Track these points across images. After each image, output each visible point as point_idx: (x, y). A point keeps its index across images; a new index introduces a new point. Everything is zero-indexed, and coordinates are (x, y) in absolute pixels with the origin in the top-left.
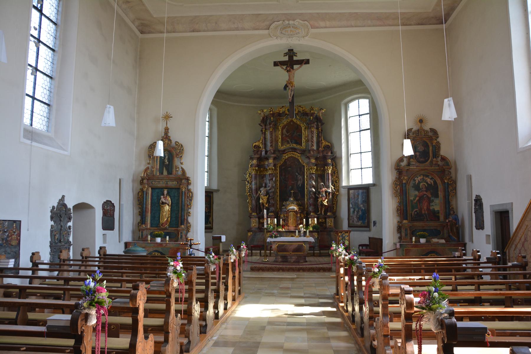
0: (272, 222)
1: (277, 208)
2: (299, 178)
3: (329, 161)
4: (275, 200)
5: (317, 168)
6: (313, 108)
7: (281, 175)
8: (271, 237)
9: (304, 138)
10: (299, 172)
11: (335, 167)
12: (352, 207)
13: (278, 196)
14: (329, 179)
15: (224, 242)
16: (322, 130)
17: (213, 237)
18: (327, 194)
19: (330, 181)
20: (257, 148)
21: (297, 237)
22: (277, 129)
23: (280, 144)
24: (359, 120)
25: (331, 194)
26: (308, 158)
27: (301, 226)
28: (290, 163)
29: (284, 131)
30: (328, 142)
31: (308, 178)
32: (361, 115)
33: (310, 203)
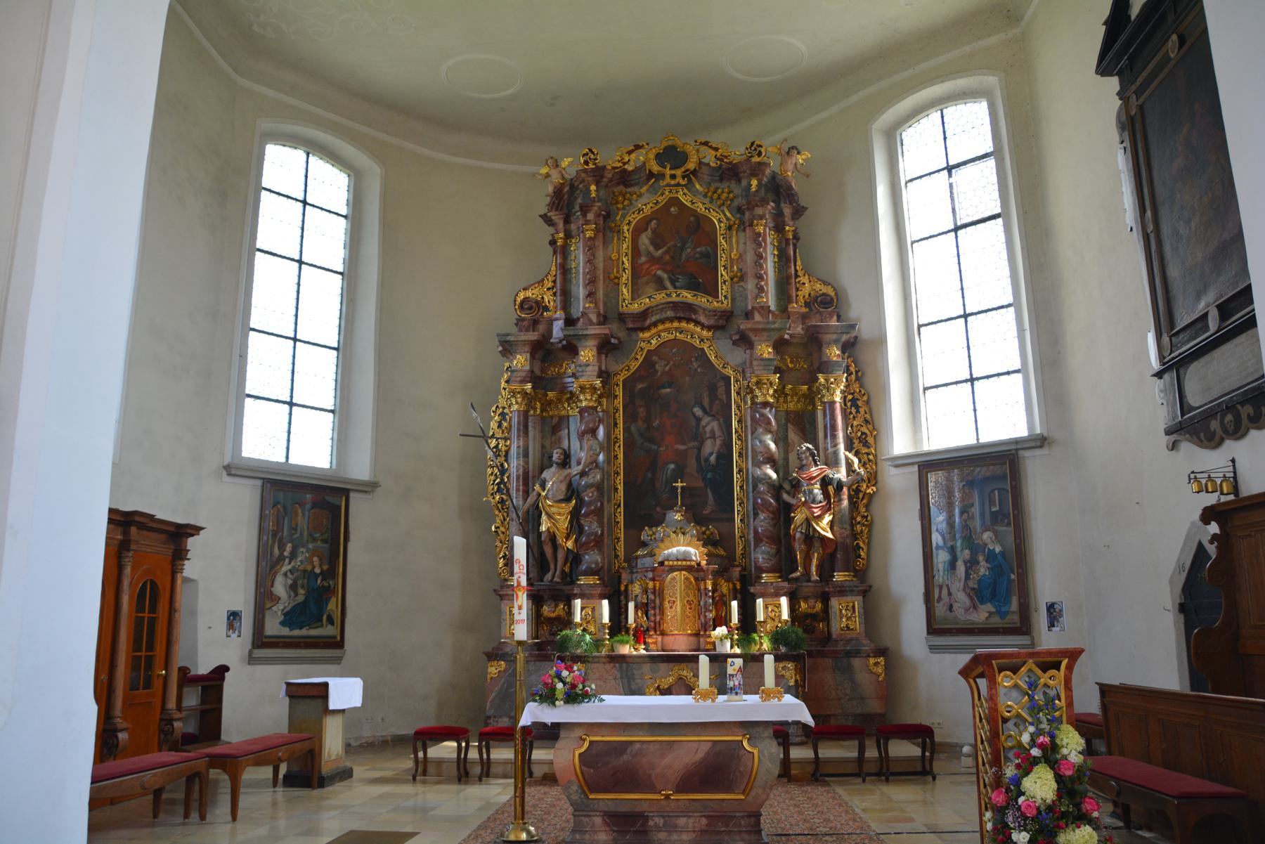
0: (593, 617)
1: (616, 556)
2: (708, 429)
3: (834, 353)
4: (606, 520)
5: (784, 388)
6: (760, 146)
7: (630, 416)
8: (548, 697)
9: (725, 268)
10: (706, 402)
11: (857, 379)
12: (941, 543)
13: (619, 506)
14: (834, 427)
15: (355, 709)
16: (796, 237)
17: (288, 684)
18: (831, 489)
19: (840, 435)
20: (531, 308)
21: (705, 696)
22: (615, 234)
23: (625, 292)
24: (951, 186)
25: (845, 490)
26: (744, 341)
27: (722, 630)
28: (667, 368)
29: (644, 240)
30: (825, 283)
31: (746, 426)
32: (958, 166)
33: (756, 531)
